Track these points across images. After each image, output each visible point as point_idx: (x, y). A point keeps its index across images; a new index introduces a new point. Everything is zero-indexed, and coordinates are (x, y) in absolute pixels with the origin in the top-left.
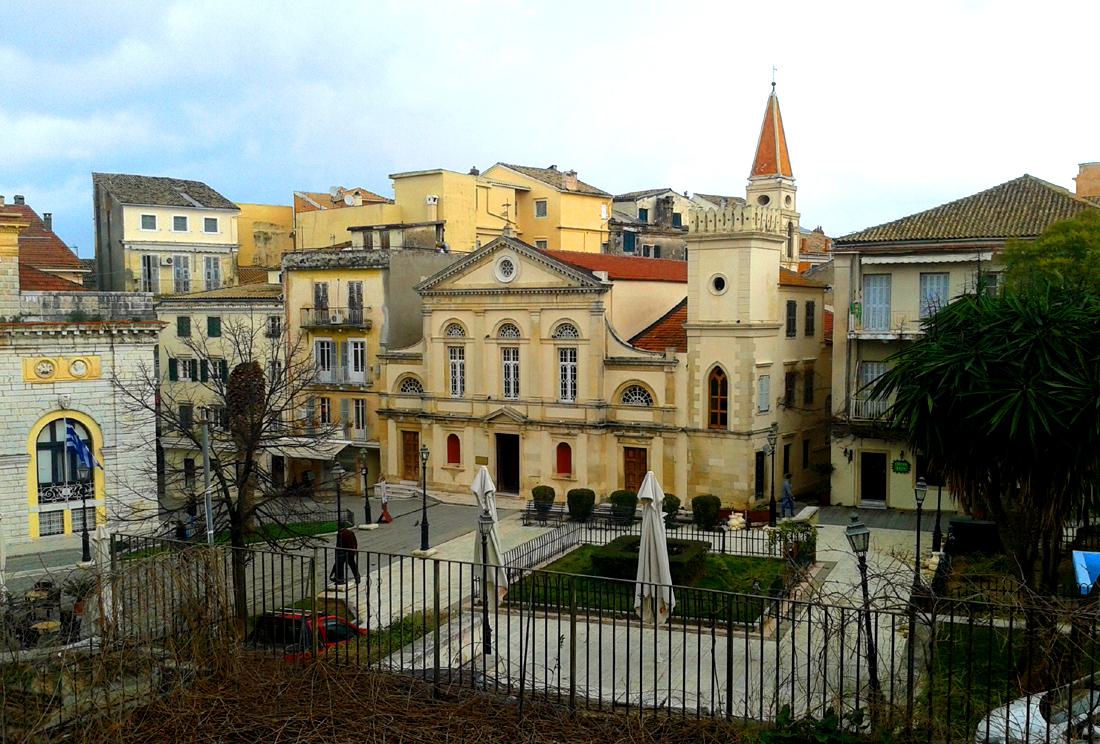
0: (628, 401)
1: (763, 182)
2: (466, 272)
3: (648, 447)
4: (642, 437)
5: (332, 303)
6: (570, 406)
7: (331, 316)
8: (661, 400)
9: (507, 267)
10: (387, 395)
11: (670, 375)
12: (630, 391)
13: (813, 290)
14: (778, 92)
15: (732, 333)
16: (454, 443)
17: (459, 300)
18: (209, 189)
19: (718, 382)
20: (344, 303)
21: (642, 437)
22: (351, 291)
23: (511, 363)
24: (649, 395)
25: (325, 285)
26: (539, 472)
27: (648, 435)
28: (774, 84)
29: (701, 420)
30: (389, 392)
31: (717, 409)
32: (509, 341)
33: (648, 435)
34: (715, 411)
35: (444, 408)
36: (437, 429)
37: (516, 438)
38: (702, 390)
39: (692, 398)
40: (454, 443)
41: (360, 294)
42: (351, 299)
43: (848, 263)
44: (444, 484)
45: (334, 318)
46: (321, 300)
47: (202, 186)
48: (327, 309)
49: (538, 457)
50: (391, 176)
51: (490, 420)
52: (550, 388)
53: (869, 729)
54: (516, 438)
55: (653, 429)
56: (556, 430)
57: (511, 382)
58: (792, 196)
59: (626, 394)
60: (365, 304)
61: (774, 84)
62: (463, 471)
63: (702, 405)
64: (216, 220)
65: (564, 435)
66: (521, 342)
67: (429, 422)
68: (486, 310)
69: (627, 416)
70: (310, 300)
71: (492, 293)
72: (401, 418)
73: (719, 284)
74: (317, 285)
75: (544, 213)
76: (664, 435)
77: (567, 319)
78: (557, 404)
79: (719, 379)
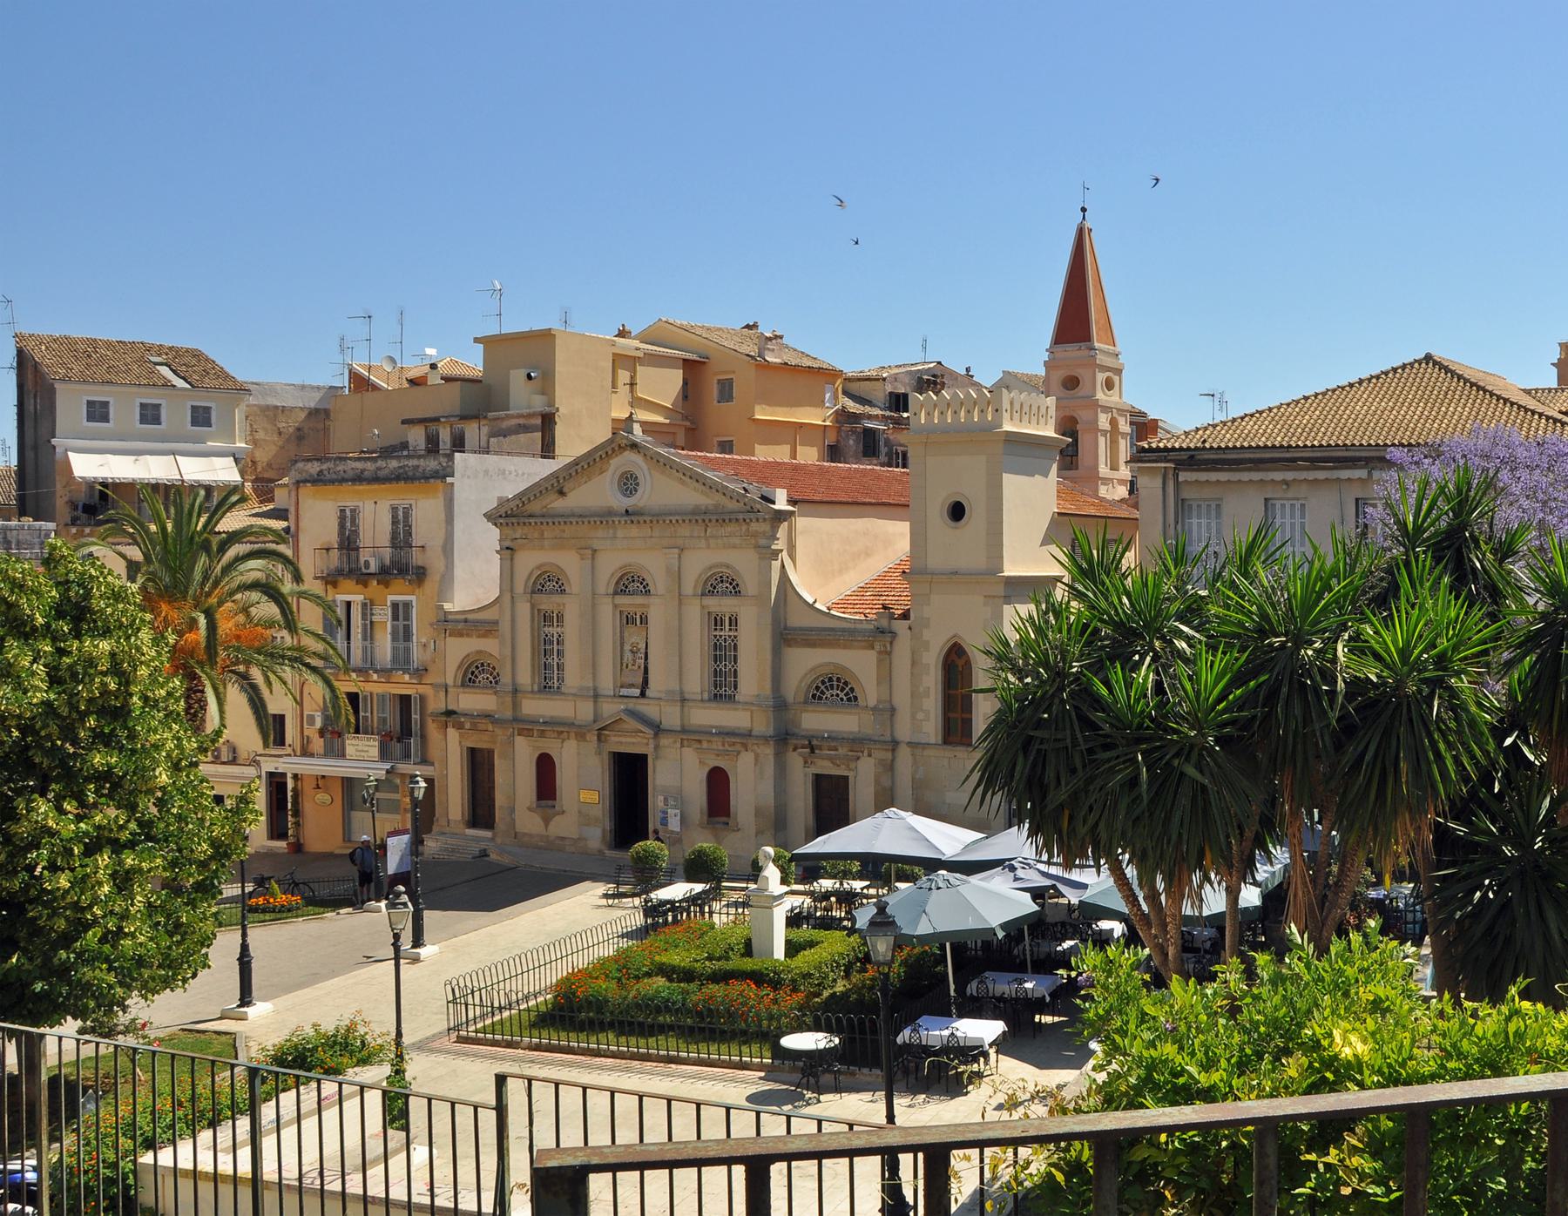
1: (1072, 351)
3: (851, 774)
5: (365, 539)
7: (362, 560)
8: (870, 693)
9: (629, 483)
13: (892, 509)
14: (1088, 224)
16: (545, 766)
18: (207, 359)
19: (955, 663)
20: (384, 538)
22: (395, 522)
24: (852, 690)
25: (353, 511)
28: (1084, 210)
37: (643, 759)
38: (933, 680)
40: (545, 766)
41: (408, 526)
42: (394, 535)
43: (1158, 482)
45: (367, 564)
46: (348, 543)
47: (197, 355)
48: (357, 549)
50: (477, 340)
52: (696, 679)
54: (643, 759)
55: (858, 744)
58: (1116, 379)
59: (817, 688)
60: (417, 540)
61: (1084, 210)
62: (563, 812)
63: (933, 704)
64: (159, 406)
69: (815, 721)
70: (333, 537)
71: (605, 517)
72: (842, 751)
73: (957, 511)
74: (342, 511)
75: (730, 398)
79: (960, 662)
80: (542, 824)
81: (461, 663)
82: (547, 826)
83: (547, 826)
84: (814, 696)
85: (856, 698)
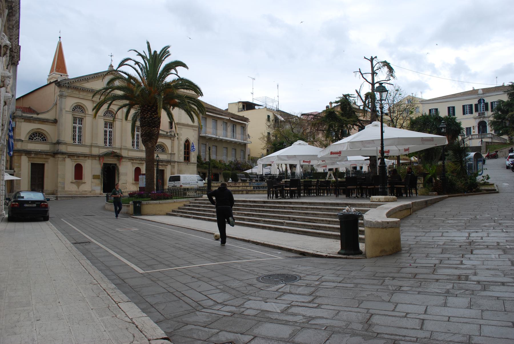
0: (32, 139)
2: (89, 81)
4: (164, 165)
6: (76, 145)
10: (22, 141)
11: (173, 141)
12: (160, 146)
15: (192, 128)
17: (85, 94)
21: (164, 165)
23: (108, 130)
26: (127, 181)
27: (166, 164)
28: (60, 38)
29: (182, 159)
30: (23, 139)
31: (187, 157)
32: (79, 115)
33: (166, 164)
34: (188, 156)
35: (71, 149)
36: (68, 161)
38: (182, 148)
39: (179, 151)
44: (72, 191)
49: (126, 174)
51: (100, 157)
53: (25, 206)
55: (169, 162)
56: (135, 161)
57: (109, 138)
61: (60, 38)
65: (138, 163)
66: (87, 115)
72: (33, 155)
76: (172, 164)
78: (129, 150)
80: (77, 187)
81: (29, 132)
82: (78, 188)
83: (78, 188)
85: (45, 140)
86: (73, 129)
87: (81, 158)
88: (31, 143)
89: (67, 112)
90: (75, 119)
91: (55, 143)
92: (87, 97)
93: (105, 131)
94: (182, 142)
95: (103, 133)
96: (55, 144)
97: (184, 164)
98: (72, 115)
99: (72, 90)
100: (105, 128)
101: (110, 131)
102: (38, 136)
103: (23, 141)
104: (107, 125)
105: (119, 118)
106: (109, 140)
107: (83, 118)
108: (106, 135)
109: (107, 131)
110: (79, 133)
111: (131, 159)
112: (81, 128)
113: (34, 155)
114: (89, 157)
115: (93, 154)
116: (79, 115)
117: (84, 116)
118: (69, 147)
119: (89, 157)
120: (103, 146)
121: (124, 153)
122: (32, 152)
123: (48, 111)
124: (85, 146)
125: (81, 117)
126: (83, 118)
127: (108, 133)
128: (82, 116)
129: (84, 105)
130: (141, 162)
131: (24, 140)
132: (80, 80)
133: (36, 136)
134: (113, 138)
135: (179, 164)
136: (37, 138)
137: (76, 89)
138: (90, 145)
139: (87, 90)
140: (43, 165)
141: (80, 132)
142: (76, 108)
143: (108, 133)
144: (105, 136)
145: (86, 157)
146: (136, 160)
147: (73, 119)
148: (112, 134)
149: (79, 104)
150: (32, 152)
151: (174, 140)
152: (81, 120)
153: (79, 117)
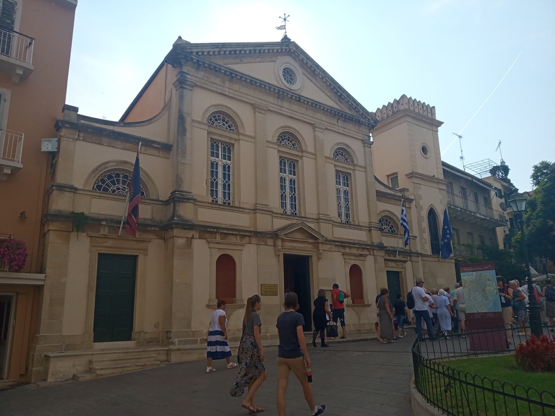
0: (106, 190)
9: (288, 74)
23: (221, 161)
38: (425, 224)
39: (421, 231)
56: (347, 250)
67: (190, 234)
68: (269, 110)
77: (348, 146)
78: (334, 223)
84: (99, 187)
86: (210, 169)
87: (233, 239)
88: (100, 197)
89: (328, 161)
90: (214, 144)
91: (167, 201)
92: (348, 131)
93: (281, 178)
94: (425, 213)
95: (335, 191)
96: (166, 203)
97: (433, 259)
98: (209, 133)
99: (206, 74)
100: (281, 172)
101: (291, 180)
102: (121, 182)
103: (76, 189)
104: (285, 166)
105: (247, 133)
106: (224, 188)
107: (233, 144)
108: (283, 187)
109: (217, 164)
110: (225, 179)
111: (342, 244)
112: (229, 167)
113: (107, 229)
114: (249, 236)
115: (258, 230)
116: (223, 134)
117: (235, 140)
118: (201, 211)
119: (249, 236)
120: (279, 211)
121: (326, 231)
122: (104, 223)
123: (150, 121)
124: (239, 209)
125: (227, 140)
126: (233, 144)
127: (287, 183)
128: (230, 138)
129: (234, 112)
130: (360, 252)
131: (79, 187)
132: (225, 52)
133: (118, 181)
134: (299, 194)
135: (425, 258)
136: (118, 189)
137: (216, 70)
138: (253, 208)
139: (261, 84)
140: (135, 258)
141: (292, 189)
142: (283, 140)
143: (287, 183)
144: (282, 189)
145: (244, 236)
146: (350, 247)
147: (210, 143)
148: (231, 173)
149: (290, 131)
150: (104, 223)
151: (410, 208)
152: (229, 149)
153: (223, 139)
